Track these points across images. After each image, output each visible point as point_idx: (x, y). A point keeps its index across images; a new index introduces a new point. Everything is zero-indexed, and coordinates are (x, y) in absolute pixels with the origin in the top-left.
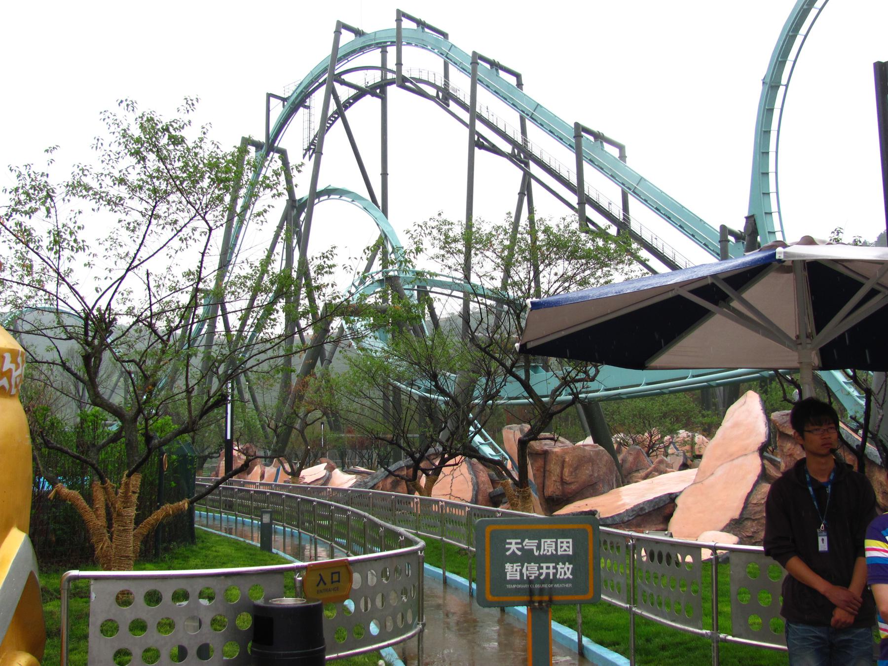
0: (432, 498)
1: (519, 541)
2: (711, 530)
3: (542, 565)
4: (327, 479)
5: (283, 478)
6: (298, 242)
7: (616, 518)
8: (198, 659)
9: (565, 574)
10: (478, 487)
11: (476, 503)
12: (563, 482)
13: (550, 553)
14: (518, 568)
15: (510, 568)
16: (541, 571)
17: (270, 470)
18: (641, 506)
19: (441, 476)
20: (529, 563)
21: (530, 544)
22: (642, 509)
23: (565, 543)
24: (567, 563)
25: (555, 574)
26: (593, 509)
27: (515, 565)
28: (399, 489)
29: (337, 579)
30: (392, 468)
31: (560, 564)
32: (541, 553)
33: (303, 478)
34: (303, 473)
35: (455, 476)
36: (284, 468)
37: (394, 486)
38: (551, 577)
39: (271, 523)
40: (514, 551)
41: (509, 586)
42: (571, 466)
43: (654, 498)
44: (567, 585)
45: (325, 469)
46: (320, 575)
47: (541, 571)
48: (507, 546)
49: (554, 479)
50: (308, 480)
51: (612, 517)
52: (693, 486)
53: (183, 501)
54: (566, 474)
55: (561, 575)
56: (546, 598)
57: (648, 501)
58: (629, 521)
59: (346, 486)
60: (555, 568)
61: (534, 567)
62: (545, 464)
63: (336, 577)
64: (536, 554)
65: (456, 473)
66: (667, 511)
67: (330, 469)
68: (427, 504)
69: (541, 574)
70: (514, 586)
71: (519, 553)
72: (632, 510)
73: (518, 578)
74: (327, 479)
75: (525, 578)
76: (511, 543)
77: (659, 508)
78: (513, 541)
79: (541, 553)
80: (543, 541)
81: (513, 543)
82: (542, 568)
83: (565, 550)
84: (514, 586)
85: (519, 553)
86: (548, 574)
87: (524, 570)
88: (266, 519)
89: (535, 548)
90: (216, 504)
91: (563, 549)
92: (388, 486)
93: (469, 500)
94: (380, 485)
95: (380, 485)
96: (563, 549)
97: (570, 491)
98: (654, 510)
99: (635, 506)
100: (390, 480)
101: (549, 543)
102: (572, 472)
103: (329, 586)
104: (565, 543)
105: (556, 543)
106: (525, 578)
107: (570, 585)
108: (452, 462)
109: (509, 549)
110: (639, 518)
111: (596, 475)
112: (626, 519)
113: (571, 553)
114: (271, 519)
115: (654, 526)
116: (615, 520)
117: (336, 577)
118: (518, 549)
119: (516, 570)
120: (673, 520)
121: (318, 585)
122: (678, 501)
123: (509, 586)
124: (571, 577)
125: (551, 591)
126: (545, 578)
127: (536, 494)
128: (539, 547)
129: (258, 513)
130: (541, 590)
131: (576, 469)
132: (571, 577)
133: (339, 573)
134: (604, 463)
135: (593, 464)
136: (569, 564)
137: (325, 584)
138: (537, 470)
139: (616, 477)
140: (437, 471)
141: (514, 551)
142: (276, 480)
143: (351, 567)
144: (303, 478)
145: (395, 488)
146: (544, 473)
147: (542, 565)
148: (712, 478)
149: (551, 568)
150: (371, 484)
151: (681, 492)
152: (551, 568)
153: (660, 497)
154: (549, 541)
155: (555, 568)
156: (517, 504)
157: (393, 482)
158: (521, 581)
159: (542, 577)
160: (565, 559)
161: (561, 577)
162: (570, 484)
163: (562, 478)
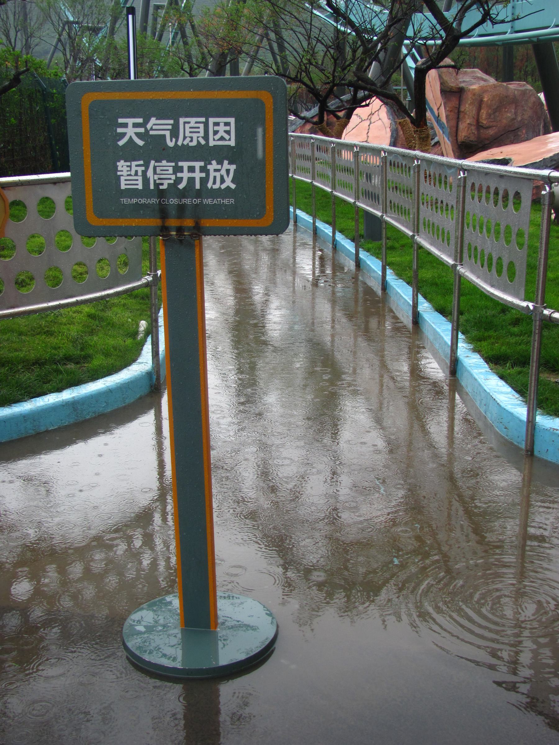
1: (140, 120)
3: (180, 164)
9: (223, 181)
13: (194, 143)
14: (140, 169)
15: (125, 169)
16: (179, 175)
19: (354, 119)
23: (222, 125)
24: (226, 162)
25: (204, 181)
27: (134, 163)
31: (214, 162)
32: (180, 143)
35: (372, 121)
38: (198, 186)
41: (125, 201)
44: (226, 201)
47: (179, 175)
48: (120, 130)
49: (468, 121)
54: (484, 116)
55: (214, 183)
56: (189, 223)
60: (203, 169)
61: (167, 166)
62: (459, 105)
64: (171, 144)
65: (374, 118)
69: (179, 180)
70: (134, 201)
71: (140, 143)
73: (140, 187)
75: (152, 187)
76: (125, 125)
78: (130, 121)
79: (180, 143)
80: (182, 120)
81: (130, 125)
82: (181, 170)
84: (134, 201)
85: (140, 143)
86: (191, 181)
87: (150, 173)
89: (168, 134)
91: (217, 137)
96: (217, 137)
99: (555, 155)
101: (192, 125)
104: (222, 125)
105: (206, 124)
106: (152, 187)
107: (232, 201)
109: (124, 135)
113: (232, 143)
119: (136, 174)
123: (125, 201)
124: (233, 186)
126: (185, 188)
127: (449, 140)
128: (175, 133)
130: (181, 209)
132: (233, 186)
134: (530, 105)
146: (458, 115)
147: (180, 164)
149: (197, 169)
152: (197, 169)
154: (193, 120)
155: (203, 169)
159: (181, 186)
161: (216, 187)
163: (478, 121)
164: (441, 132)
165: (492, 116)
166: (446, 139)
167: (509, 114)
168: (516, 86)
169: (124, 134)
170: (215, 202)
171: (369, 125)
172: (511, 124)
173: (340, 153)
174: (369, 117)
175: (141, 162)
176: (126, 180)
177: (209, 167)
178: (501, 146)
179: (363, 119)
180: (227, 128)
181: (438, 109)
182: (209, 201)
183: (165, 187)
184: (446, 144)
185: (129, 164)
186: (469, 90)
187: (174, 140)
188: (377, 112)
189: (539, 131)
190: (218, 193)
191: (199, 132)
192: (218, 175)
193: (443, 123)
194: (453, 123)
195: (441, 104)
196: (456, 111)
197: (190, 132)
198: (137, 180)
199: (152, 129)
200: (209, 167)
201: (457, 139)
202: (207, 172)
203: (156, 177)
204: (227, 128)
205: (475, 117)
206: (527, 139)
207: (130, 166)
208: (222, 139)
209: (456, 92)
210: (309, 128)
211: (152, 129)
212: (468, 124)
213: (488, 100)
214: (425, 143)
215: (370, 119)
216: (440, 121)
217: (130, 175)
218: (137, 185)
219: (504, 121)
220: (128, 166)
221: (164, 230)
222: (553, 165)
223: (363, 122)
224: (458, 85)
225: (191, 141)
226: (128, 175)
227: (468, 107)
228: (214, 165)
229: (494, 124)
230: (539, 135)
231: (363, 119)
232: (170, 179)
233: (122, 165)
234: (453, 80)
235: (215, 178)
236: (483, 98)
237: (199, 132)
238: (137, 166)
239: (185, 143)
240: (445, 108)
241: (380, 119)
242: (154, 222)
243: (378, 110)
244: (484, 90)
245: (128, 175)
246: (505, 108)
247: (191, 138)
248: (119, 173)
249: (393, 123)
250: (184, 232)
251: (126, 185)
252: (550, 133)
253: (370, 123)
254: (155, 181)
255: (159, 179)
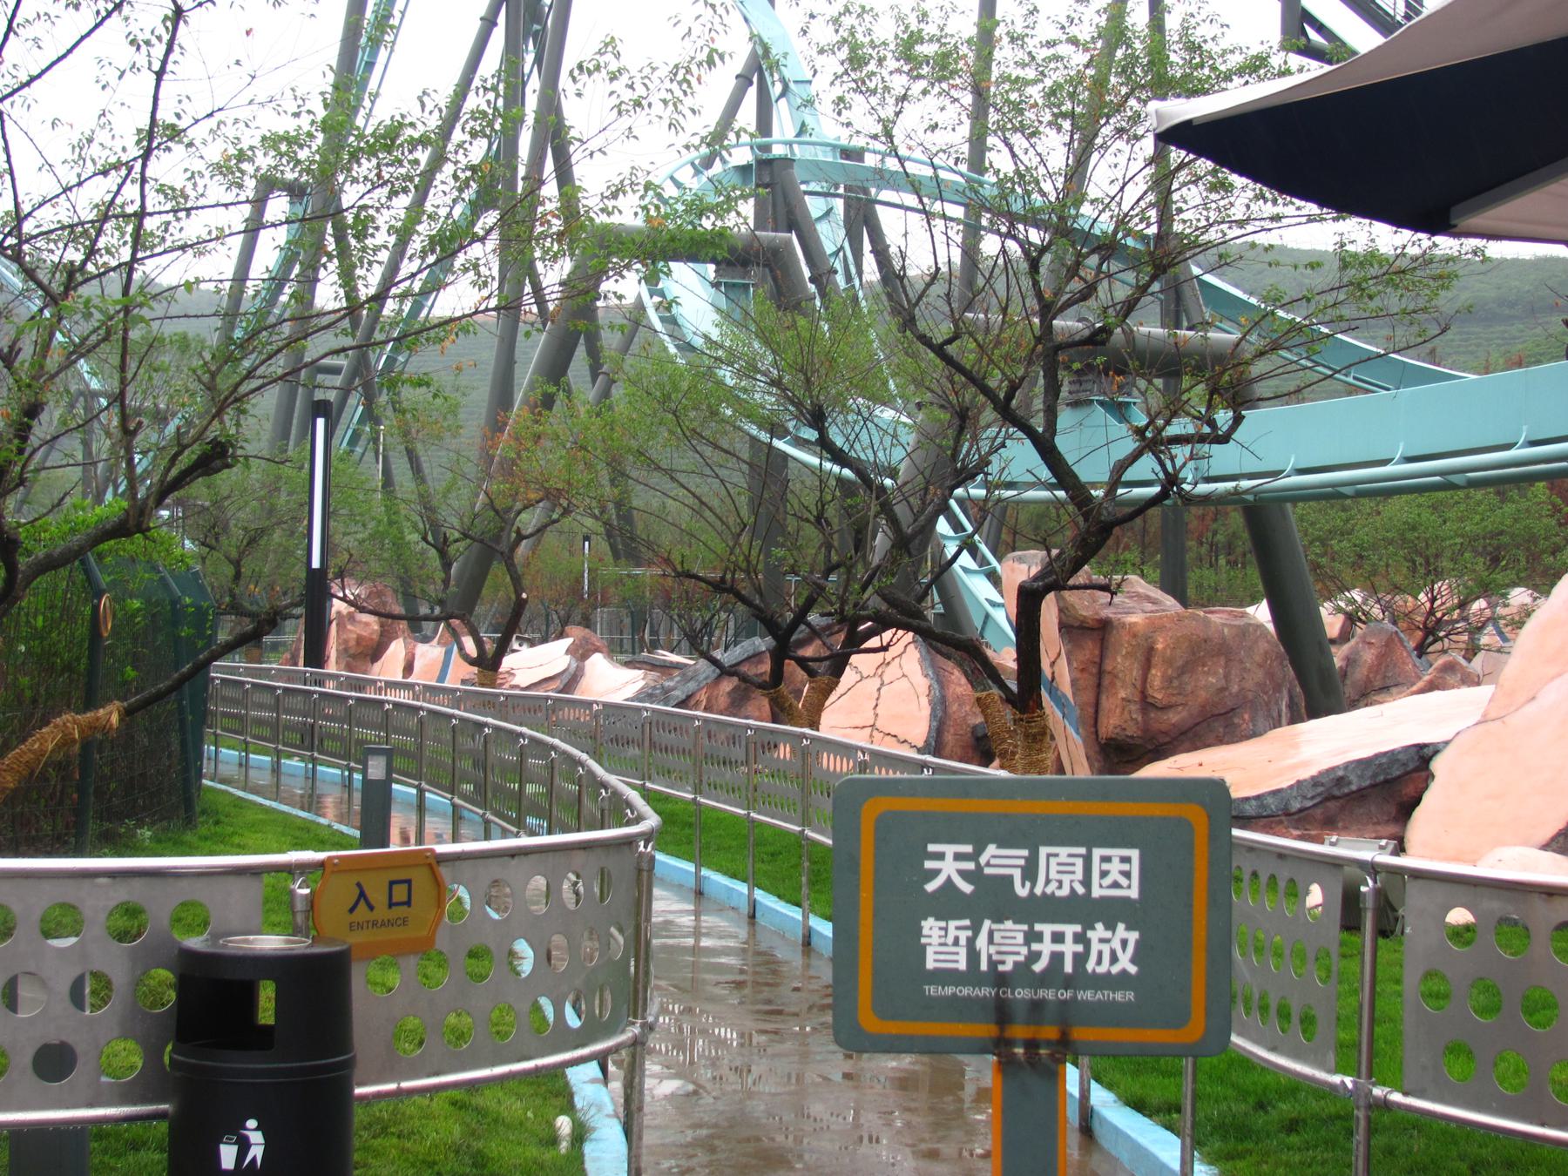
0: (825, 732)
1: (968, 849)
2: (1515, 845)
3: (1038, 927)
4: (571, 680)
5: (460, 674)
6: (538, 60)
7: (1270, 800)
8: (35, 1079)
9: (1114, 959)
10: (945, 711)
11: (937, 752)
12: (1146, 703)
13: (1065, 892)
14: (964, 936)
15: (936, 933)
16: (1035, 947)
17: (429, 654)
18: (1340, 773)
19: (848, 676)
20: (999, 920)
21: (1001, 860)
22: (1340, 781)
23: (1116, 860)
24: (1121, 927)
25: (1080, 959)
26: (1216, 775)
27: (953, 924)
28: (750, 708)
29: (405, 898)
30: (726, 657)
31: (1099, 926)
32: (1038, 891)
33: (510, 673)
34: (508, 662)
35: (886, 679)
36: (461, 648)
37: (737, 704)
38: (1068, 967)
39: (388, 781)
40: (949, 879)
41: (932, 990)
42: (1169, 662)
43: (1377, 756)
44: (1119, 996)
45: (568, 652)
46: (359, 885)
47: (1035, 947)
48: (929, 864)
49: (1122, 694)
50: (523, 678)
51: (1258, 797)
52: (1481, 728)
53: (109, 708)
54: (1157, 683)
55: (1099, 962)
56: (1050, 1032)
57: (1360, 762)
58: (1301, 811)
59: (618, 698)
60: (1080, 938)
61: (1012, 931)
62: (1102, 657)
63: (400, 893)
64: (1022, 891)
65: (891, 672)
66: (1409, 790)
67: (581, 653)
68: (809, 752)
69: (1034, 957)
70: (949, 990)
71: (966, 888)
72: (1315, 781)
73: (962, 965)
74: (571, 680)
75: (984, 966)
76: (940, 856)
77: (1386, 781)
78: (950, 849)
79: (1038, 891)
80: (1044, 851)
81: (949, 857)
82: (1039, 937)
83: (1116, 885)
84: (949, 990)
85: (966, 888)
86: (1057, 958)
87: (981, 942)
88: (377, 769)
89: (1017, 874)
90: (267, 732)
91: (1107, 881)
92: (723, 701)
93: (920, 744)
94: (703, 697)
95: (703, 697)
96: (1107, 881)
97: (1164, 727)
98: (1373, 786)
99: (1321, 774)
100: (728, 685)
101: (1063, 858)
102: (1170, 680)
103: (382, 912)
104: (1116, 860)
105: (1088, 860)
106: (984, 966)
107: (1130, 995)
108: (874, 642)
109: (935, 873)
110: (1332, 805)
111: (1235, 689)
112: (1296, 805)
113: (1134, 893)
114: (390, 770)
115: (1370, 827)
116: (1263, 806)
117: (400, 893)
118: (963, 874)
119: (956, 942)
120: (1419, 813)
121: (352, 910)
122: (1437, 765)
123: (932, 990)
124: (1133, 969)
125: (1066, 1014)
126: (1045, 972)
127: (1077, 732)
128: (1030, 872)
129: (354, 753)
130: (1037, 1006)
131: (1182, 671)
132: (1133, 969)
133: (409, 882)
134: (1258, 658)
135: (1228, 660)
136: (1128, 928)
137: (371, 908)
138: (1083, 670)
139: (1291, 698)
140: (838, 665)
141: (949, 879)
142: (442, 678)
143: (444, 872)
144: (510, 673)
145: (739, 706)
146: (1100, 679)
147: (1038, 927)
148: (1530, 709)
149: (1069, 938)
150: (679, 694)
151: (1447, 743)
152: (1069, 938)
153: (1392, 752)
154: (1063, 851)
155: (1080, 938)
156: (1014, 754)
157: (735, 689)
158: (972, 975)
159: (1038, 967)
160: (1111, 912)
161: (1102, 969)
162: (1164, 708)
163: (1144, 695)
164: (1060, 715)
165: (1176, 683)
166: (1071, 730)
167: (1208, 680)
168: (1225, 616)
169: (936, 872)
170: (1099, 995)
171: (879, 690)
172: (1216, 699)
173: (818, 756)
174: (880, 671)
175: (967, 922)
176: (936, 953)
177: (1090, 934)
178: (1196, 748)
179: (865, 675)
180: (1126, 867)
181: (1053, 664)
182: (1087, 995)
183: (1008, 967)
184: (1070, 743)
185: (943, 924)
186: (1123, 625)
187: (1028, 884)
188: (897, 660)
189: (1280, 716)
190: (1107, 981)
191: (1073, 872)
192: (1106, 949)
193: (1065, 696)
194: (1089, 696)
195: (1059, 654)
196: (1095, 670)
197: (1059, 872)
198: (957, 953)
199: (988, 864)
200: (1090, 934)
201: (1097, 732)
202: (1087, 943)
203: (993, 949)
204: (1126, 867)
205: (1138, 684)
206: (1255, 734)
207: (946, 929)
208: (1116, 885)
209: (1092, 629)
210: (728, 689)
211: (988, 864)
212: (1123, 699)
213: (1164, 648)
214: (1038, 747)
215: (881, 676)
216: (1057, 689)
217: (945, 944)
218: (957, 961)
219: (1203, 694)
220: (941, 929)
221: (1000, 1045)
222: (1319, 795)
223: (864, 681)
224: (1097, 614)
225: (1060, 887)
226: (941, 945)
227: (1122, 663)
228: (1099, 931)
229: (1180, 699)
230: (1280, 726)
231: (865, 675)
232: (1018, 953)
233: (930, 926)
234: (1087, 605)
235: (1100, 954)
236: (1154, 643)
237: (1073, 872)
238: (958, 928)
239: (1049, 890)
240: (1069, 663)
241: (904, 675)
242: (987, 1030)
243: (900, 655)
244: (1155, 627)
245: (941, 945)
246: (1204, 666)
247: (1060, 883)
248: (923, 940)
249: (936, 686)
250: (1015, 1047)
251: (936, 961)
252: (1302, 721)
253: (882, 684)
254: (990, 956)
255: (999, 953)
